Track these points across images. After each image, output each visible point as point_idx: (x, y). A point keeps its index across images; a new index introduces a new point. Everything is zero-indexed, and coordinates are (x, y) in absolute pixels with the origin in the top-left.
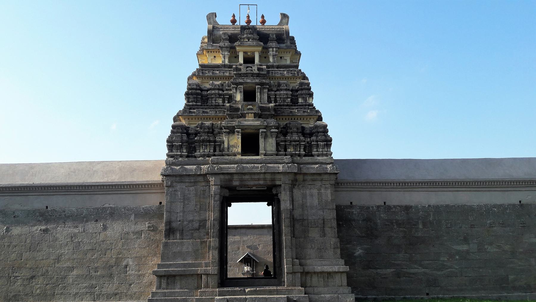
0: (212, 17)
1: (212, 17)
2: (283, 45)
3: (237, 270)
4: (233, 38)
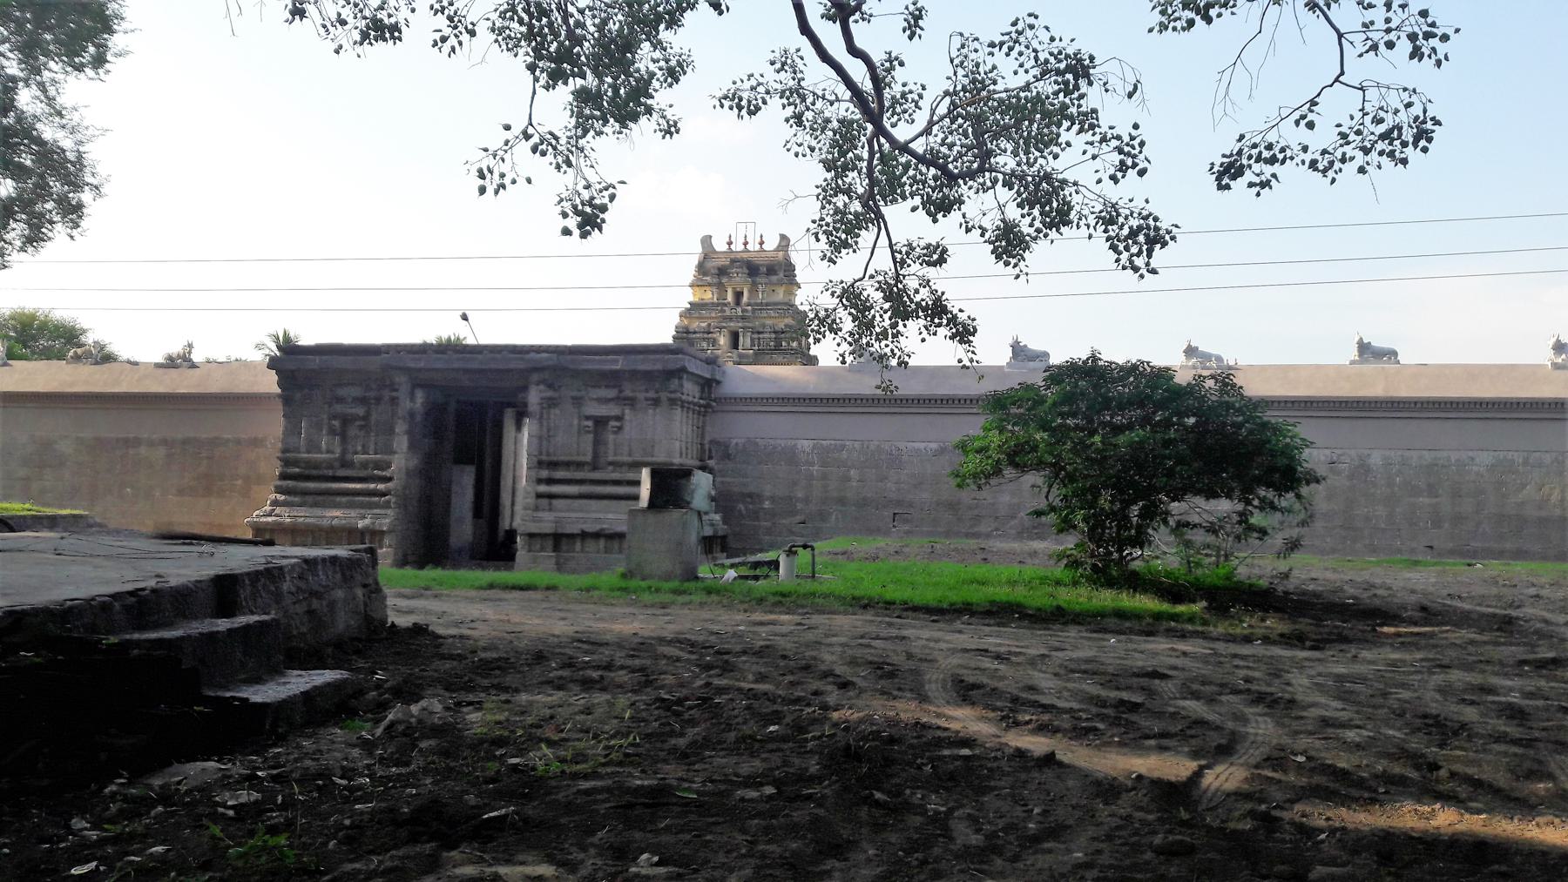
0: (707, 241)
1: (707, 241)
2: (774, 278)
4: (722, 272)
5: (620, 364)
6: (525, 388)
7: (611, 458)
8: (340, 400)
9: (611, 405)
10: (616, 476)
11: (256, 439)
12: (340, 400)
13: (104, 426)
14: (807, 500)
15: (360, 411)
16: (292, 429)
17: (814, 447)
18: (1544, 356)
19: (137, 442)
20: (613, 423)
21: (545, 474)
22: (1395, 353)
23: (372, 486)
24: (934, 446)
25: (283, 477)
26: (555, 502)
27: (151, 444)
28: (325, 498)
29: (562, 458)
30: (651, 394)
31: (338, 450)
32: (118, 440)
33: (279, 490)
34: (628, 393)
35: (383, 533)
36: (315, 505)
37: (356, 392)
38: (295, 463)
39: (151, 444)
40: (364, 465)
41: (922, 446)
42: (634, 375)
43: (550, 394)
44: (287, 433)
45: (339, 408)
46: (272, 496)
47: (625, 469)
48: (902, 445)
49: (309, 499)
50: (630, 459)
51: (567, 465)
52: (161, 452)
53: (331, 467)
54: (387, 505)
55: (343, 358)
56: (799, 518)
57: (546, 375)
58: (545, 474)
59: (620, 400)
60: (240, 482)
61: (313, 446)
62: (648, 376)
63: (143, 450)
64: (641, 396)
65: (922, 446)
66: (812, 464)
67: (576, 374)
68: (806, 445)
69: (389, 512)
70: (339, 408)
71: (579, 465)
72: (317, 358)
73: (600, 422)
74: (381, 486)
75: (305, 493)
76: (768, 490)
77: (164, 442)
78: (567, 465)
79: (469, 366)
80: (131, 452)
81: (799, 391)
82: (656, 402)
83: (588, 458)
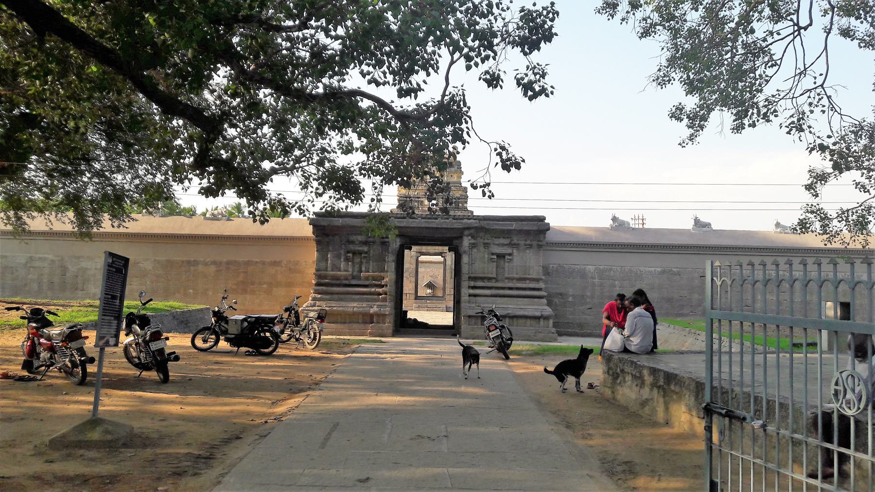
3: (423, 292)
5: (514, 226)
6: (460, 238)
7: (506, 275)
8: (353, 242)
9: (505, 247)
10: (510, 285)
11: (275, 262)
12: (353, 242)
13: (177, 254)
14: (592, 297)
15: (366, 249)
16: (323, 258)
17: (596, 269)
18: (689, 225)
19: (196, 263)
20: (507, 257)
21: (472, 284)
22: (710, 224)
23: (373, 290)
24: (659, 269)
25: (318, 284)
26: (478, 298)
27: (206, 264)
28: (341, 297)
29: (480, 275)
30: (528, 242)
31: (350, 270)
32: (183, 262)
33: (316, 292)
34: (515, 241)
35: (385, 315)
36: (341, 300)
37: (360, 238)
38: (325, 277)
39: (206, 264)
40: (367, 278)
41: (653, 269)
42: (520, 232)
43: (473, 241)
44: (319, 261)
45: (352, 247)
46: (313, 295)
47: (515, 281)
48: (642, 269)
49: (336, 296)
50: (517, 276)
51: (482, 279)
52: (213, 268)
53: (346, 279)
54: (384, 300)
55: (351, 219)
56: (588, 306)
57: (472, 231)
58: (472, 284)
59: (511, 245)
60: (265, 286)
61: (336, 268)
62: (527, 233)
63: (200, 268)
64: (522, 243)
65: (653, 269)
66: (594, 278)
67: (486, 230)
68: (591, 268)
69: (387, 304)
70: (352, 247)
71: (489, 279)
72: (341, 220)
73: (501, 256)
74: (380, 290)
75: (332, 294)
76: (571, 291)
77: (214, 263)
78: (482, 279)
79: (431, 226)
80: (192, 268)
81: (587, 240)
82: (531, 246)
83: (494, 276)
